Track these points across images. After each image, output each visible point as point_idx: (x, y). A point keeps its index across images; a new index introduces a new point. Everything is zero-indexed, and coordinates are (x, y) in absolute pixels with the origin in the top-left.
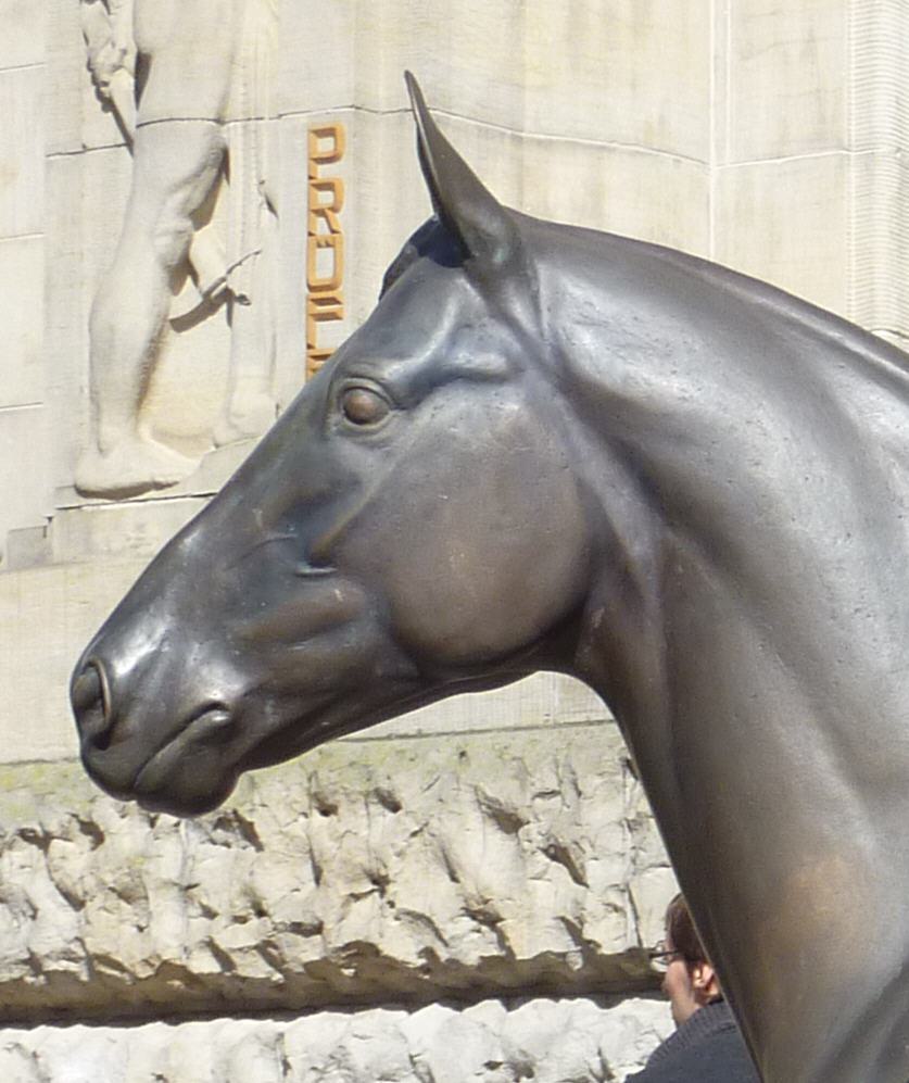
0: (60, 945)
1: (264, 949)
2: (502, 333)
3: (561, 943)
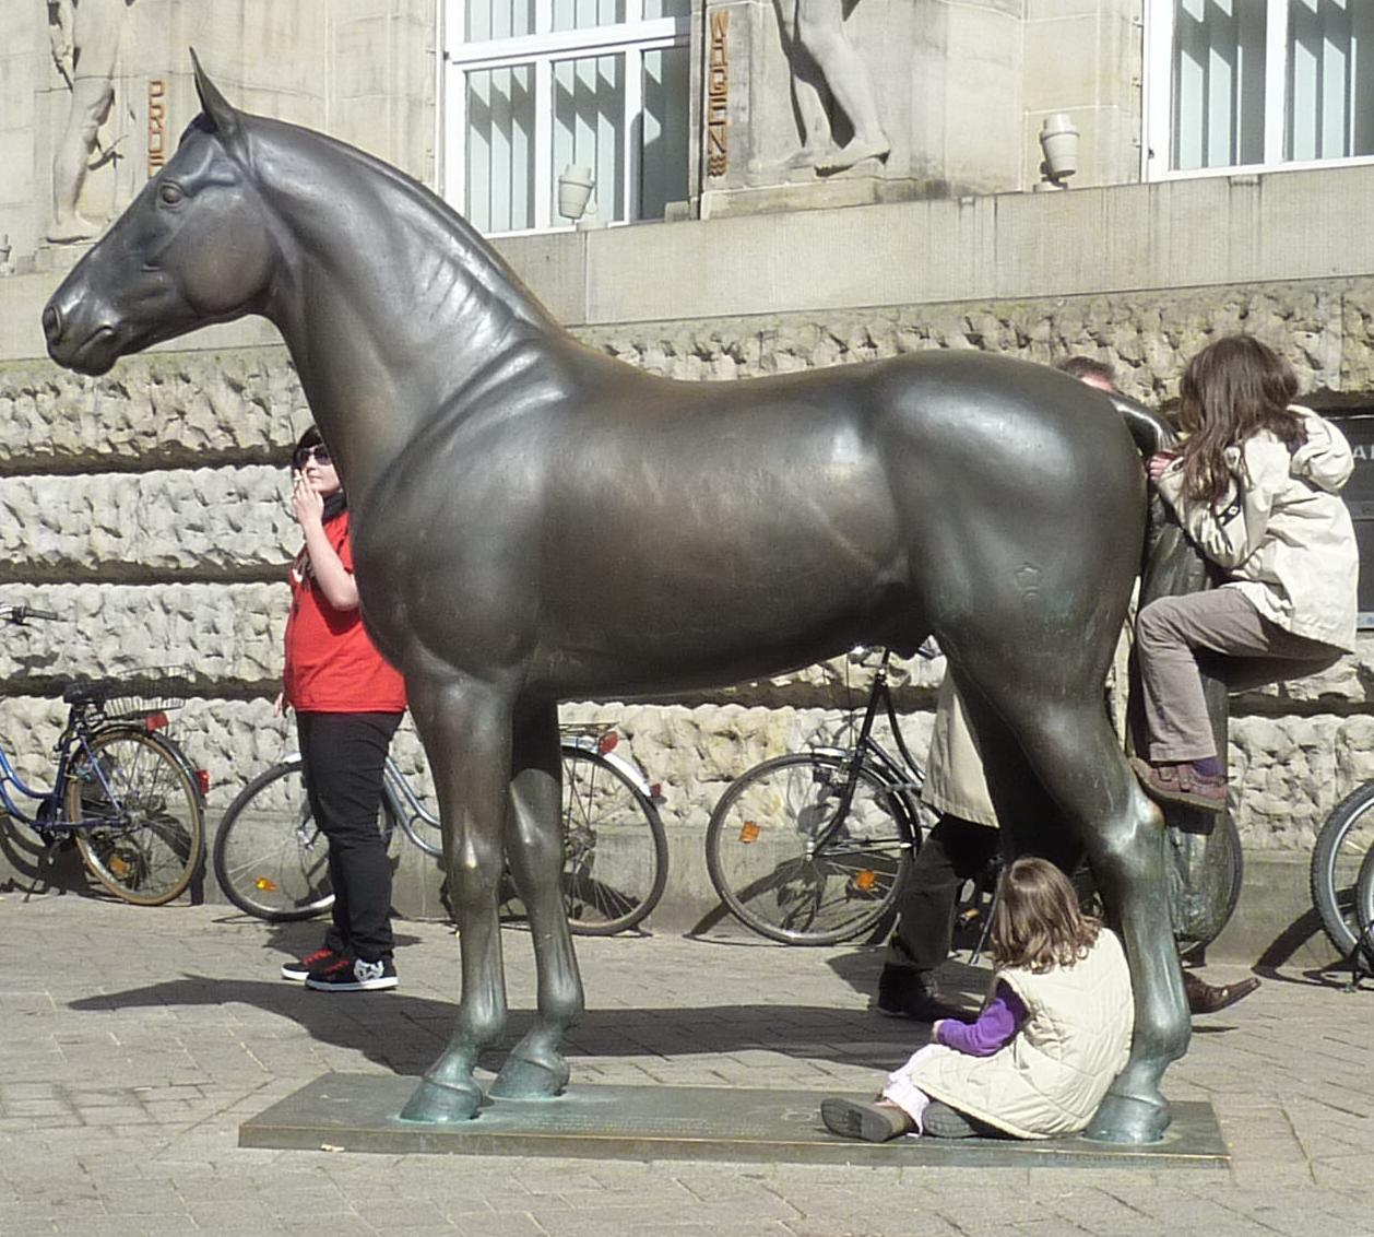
0: (41, 440)
1: (131, 442)
2: (233, 164)
3: (260, 441)
